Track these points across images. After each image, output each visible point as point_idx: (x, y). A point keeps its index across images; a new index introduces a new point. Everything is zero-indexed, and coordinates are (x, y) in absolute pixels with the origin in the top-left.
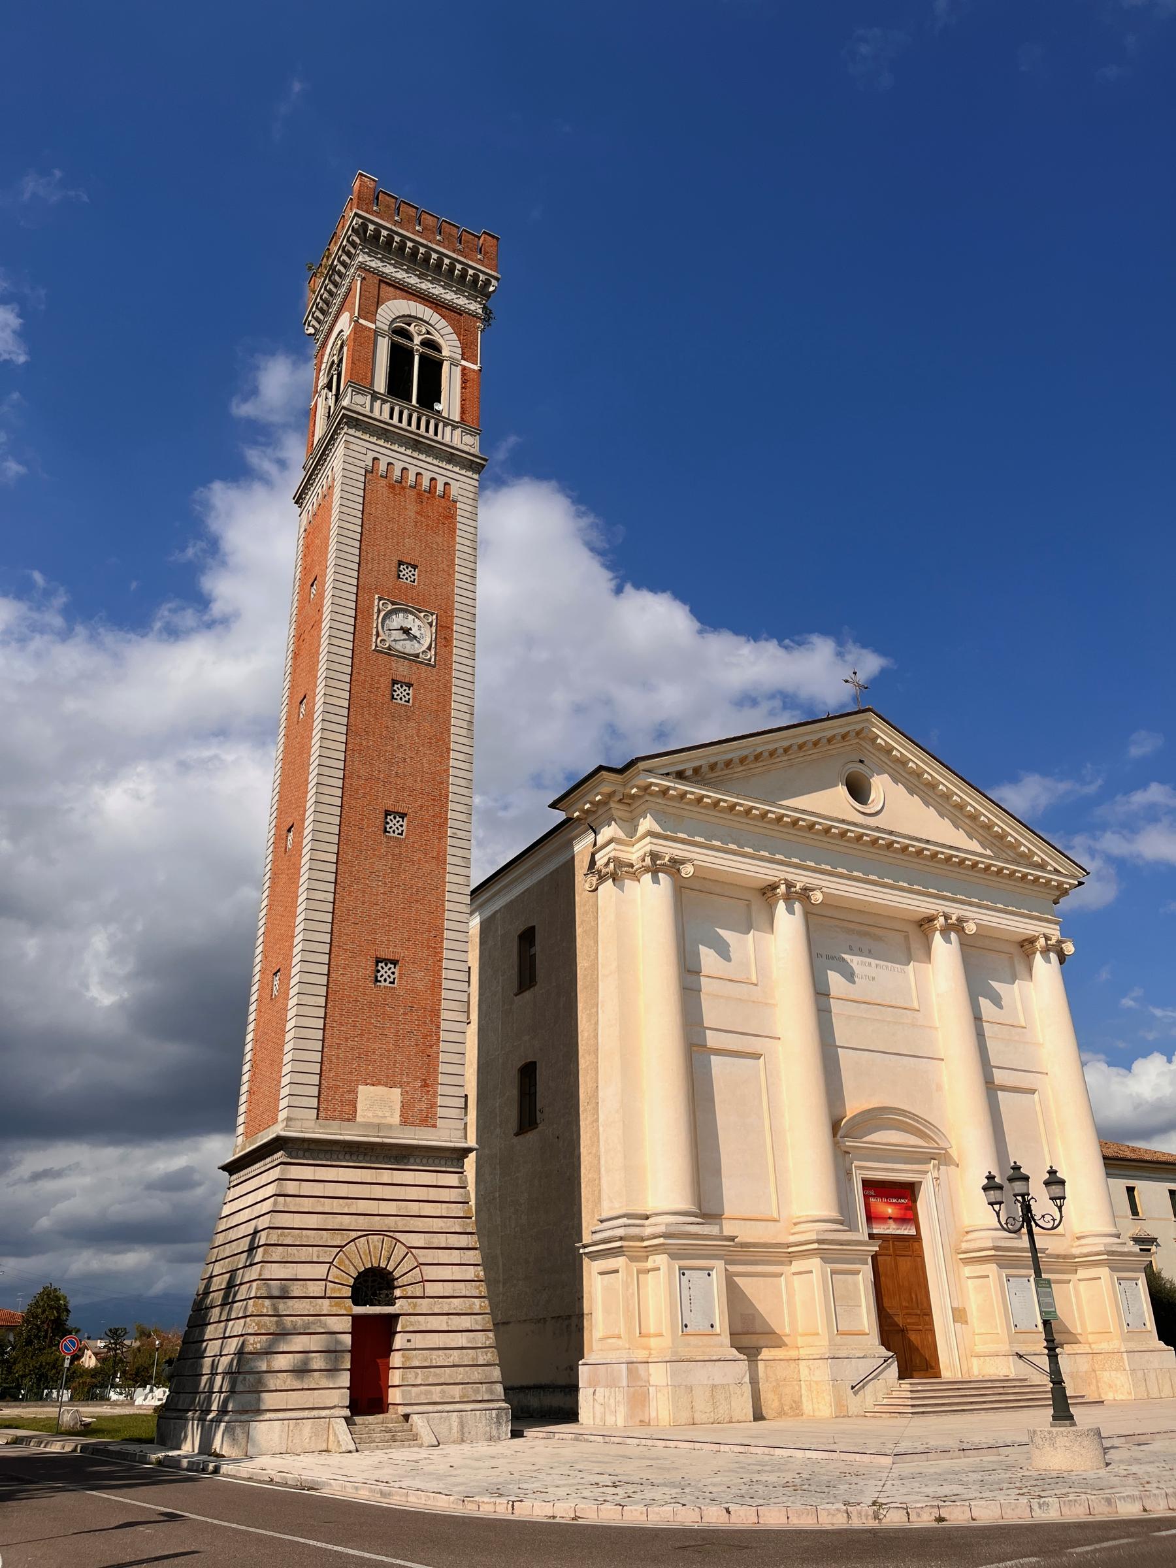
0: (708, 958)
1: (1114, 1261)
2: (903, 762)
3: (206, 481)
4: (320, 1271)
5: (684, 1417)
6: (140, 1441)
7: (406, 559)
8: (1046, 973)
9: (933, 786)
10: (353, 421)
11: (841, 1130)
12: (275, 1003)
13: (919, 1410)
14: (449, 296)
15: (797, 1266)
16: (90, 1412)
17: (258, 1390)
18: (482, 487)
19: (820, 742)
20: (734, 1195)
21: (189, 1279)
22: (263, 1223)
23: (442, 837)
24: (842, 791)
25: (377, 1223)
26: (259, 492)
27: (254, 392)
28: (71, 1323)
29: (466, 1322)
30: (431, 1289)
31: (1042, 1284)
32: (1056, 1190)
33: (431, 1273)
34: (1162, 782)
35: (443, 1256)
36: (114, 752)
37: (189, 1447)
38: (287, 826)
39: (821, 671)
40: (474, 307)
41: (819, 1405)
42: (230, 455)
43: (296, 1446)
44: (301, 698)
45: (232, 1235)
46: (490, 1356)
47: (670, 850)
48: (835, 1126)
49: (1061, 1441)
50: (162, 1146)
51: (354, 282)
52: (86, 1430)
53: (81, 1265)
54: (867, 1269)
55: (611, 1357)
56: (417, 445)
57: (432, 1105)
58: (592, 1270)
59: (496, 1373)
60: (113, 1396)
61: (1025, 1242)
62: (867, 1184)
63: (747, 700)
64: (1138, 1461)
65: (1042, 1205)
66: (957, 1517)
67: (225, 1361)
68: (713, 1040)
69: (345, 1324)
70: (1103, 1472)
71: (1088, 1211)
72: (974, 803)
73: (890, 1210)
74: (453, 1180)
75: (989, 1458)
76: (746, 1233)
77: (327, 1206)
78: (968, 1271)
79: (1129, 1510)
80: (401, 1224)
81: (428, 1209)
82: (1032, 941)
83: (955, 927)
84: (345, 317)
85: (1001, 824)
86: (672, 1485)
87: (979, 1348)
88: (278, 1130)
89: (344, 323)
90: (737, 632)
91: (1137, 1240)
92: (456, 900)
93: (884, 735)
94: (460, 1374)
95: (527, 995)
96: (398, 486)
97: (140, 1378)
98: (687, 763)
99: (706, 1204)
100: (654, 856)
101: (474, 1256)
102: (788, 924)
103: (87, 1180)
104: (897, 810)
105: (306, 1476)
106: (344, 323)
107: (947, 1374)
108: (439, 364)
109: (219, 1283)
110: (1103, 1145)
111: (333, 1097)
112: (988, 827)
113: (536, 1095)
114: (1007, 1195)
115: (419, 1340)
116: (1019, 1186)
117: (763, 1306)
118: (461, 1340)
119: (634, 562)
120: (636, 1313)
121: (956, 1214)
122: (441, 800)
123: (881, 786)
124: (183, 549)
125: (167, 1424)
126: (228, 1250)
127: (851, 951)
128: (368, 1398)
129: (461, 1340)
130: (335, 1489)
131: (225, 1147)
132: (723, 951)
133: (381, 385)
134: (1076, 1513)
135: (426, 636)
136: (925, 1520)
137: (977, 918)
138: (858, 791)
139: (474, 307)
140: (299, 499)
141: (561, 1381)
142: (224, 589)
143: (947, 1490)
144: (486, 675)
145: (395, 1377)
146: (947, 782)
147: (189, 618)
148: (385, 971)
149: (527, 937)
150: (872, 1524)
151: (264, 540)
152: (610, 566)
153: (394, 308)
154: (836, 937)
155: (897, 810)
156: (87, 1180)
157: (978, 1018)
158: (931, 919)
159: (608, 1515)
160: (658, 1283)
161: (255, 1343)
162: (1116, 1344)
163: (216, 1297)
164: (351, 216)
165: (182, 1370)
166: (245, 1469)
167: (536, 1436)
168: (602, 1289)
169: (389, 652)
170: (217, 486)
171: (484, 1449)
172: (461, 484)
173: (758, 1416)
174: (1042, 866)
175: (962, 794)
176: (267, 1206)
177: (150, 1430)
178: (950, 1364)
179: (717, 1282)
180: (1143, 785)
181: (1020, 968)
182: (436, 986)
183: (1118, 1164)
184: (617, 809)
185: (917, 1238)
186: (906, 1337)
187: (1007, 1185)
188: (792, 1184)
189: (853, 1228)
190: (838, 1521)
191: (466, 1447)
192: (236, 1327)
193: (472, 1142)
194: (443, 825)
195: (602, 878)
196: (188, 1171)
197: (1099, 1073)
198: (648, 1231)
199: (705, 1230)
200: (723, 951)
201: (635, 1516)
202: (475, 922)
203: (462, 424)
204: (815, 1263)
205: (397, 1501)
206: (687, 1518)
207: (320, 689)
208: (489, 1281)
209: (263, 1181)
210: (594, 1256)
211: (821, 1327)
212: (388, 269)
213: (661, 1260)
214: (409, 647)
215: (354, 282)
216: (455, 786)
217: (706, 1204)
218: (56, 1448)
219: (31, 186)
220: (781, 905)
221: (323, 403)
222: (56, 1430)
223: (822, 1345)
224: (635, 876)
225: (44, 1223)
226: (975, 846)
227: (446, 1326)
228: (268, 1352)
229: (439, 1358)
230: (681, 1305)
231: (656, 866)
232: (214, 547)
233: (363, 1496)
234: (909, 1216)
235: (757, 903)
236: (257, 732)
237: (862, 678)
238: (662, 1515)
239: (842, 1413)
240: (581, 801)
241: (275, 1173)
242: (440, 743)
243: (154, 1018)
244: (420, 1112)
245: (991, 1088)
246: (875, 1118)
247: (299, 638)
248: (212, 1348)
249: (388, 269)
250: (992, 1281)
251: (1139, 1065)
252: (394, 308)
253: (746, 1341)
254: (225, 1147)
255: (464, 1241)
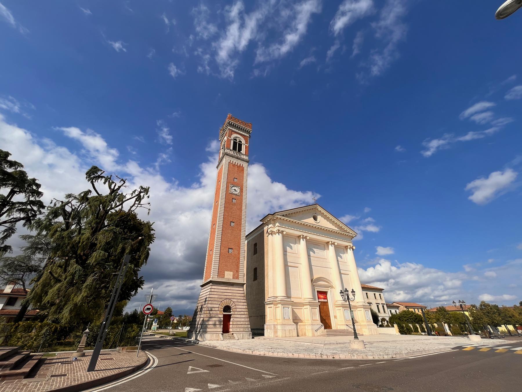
0: (288, 249)
1: (364, 307)
2: (323, 214)
3: (201, 163)
4: (217, 306)
5: (284, 335)
6: (184, 337)
7: (235, 177)
8: (350, 252)
9: (329, 218)
10: (227, 154)
11: (313, 281)
12: (211, 256)
13: (328, 335)
14: (243, 133)
15: (305, 307)
16: (175, 331)
17: (206, 328)
18: (248, 165)
19: (309, 210)
20: (293, 294)
21: (194, 306)
22: (207, 296)
23: (241, 226)
24: (312, 218)
25: (228, 297)
26: (211, 165)
27: (210, 147)
28: (172, 314)
29: (244, 316)
30: (238, 310)
31: (351, 311)
32: (353, 293)
33: (237, 307)
34: (371, 217)
35: (240, 304)
36: (183, 209)
37: (193, 339)
38: (214, 224)
39: (309, 197)
40: (247, 135)
41: (309, 334)
42: (205, 158)
43: (212, 339)
44: (216, 201)
45: (202, 298)
46: (248, 323)
47: (281, 229)
48: (312, 280)
49: (356, 343)
50: (189, 281)
51: (227, 131)
52: (174, 335)
53: (173, 303)
54: (318, 308)
55: (271, 324)
56: (237, 158)
57: (238, 275)
58: (267, 307)
59: (249, 326)
60: (179, 328)
61: (348, 303)
62: (318, 292)
63: (296, 202)
64: (371, 347)
65: (351, 296)
66: (337, 357)
67: (200, 322)
68: (289, 264)
69: (222, 316)
70: (365, 349)
71: (359, 298)
72: (336, 221)
73: (322, 297)
74: (242, 289)
75: (342, 345)
76: (296, 301)
77: (219, 293)
78: (337, 308)
79: (370, 358)
80: (232, 297)
81: (237, 295)
82: (347, 246)
83: (334, 244)
84: (226, 137)
85: (341, 225)
86: (282, 349)
87: (339, 324)
88: (210, 279)
89: (226, 138)
90: (294, 190)
91: (368, 303)
92: (243, 238)
93: (320, 209)
94: (243, 326)
95: (255, 255)
96: (234, 165)
97: (184, 325)
98: (284, 213)
99: (288, 295)
100: (279, 230)
101: (245, 304)
102: (303, 243)
103: (176, 287)
104: (322, 222)
105: (214, 345)
106: (226, 138)
107: (333, 328)
108: (241, 145)
109: (200, 307)
110: (361, 285)
111: (221, 273)
112: (339, 225)
113: (257, 274)
114: (344, 294)
115: (235, 319)
116: (347, 293)
117: (299, 315)
118: (243, 320)
119: (275, 177)
120: (275, 315)
121: (334, 298)
122: (241, 220)
123: (319, 218)
124: (198, 174)
125: (190, 332)
126: (201, 301)
127: (314, 248)
128: (226, 330)
129: (243, 320)
130: (220, 348)
131: (200, 282)
132: (291, 248)
133: (232, 148)
134: (360, 358)
135: (238, 191)
136: (331, 358)
137: (337, 242)
138: (315, 219)
139: (247, 135)
140: (217, 168)
141: (261, 328)
142: (204, 181)
143: (334, 352)
144: (249, 197)
145: (231, 326)
146: (331, 217)
147: (197, 186)
148: (230, 250)
149: (255, 245)
150: (321, 358)
151: (211, 172)
152: (271, 178)
153: (234, 136)
154: (311, 245)
155: (322, 222)
156: (176, 287)
157: (338, 261)
158: (329, 242)
159: (270, 354)
160: (279, 310)
161: (206, 319)
162: (365, 323)
163: (199, 310)
164: (227, 121)
165: (192, 323)
166: (203, 343)
167: (256, 338)
168: (269, 311)
169: (232, 193)
170: (203, 164)
171: (247, 340)
172: (245, 165)
173: (298, 336)
174: (349, 233)
175: (334, 219)
176: (208, 293)
177: (186, 335)
178: (334, 327)
179: (290, 309)
180: (367, 218)
181: (345, 251)
182: (239, 253)
183: (364, 288)
184: (272, 222)
185: (327, 302)
186: (325, 321)
187: (344, 292)
188: (304, 292)
189: (315, 300)
190: (314, 357)
191: (243, 340)
192: (202, 316)
193: (245, 282)
194: (241, 224)
195: (269, 234)
196: (194, 286)
197: (361, 271)
198: (277, 300)
199: (288, 300)
200: (291, 248)
201: (275, 355)
202: (246, 242)
203: (245, 155)
204: (308, 307)
205: (231, 350)
206: (285, 355)
207: (220, 200)
208: (248, 309)
209: (208, 287)
210: (267, 304)
211: (310, 319)
212: (233, 129)
213: (280, 305)
214: (236, 193)
215: (227, 131)
216: (243, 217)
217: (288, 295)
218: (169, 338)
219: (175, 114)
220: (302, 239)
221: (222, 151)
222: (169, 335)
223: (310, 322)
224: (275, 234)
225: (168, 295)
226: (336, 229)
227: (240, 317)
228: (208, 321)
229: (239, 323)
230: (283, 314)
231: (279, 232)
232: (203, 174)
233: (225, 349)
234: (326, 298)
235: (297, 239)
236: (210, 208)
237: (316, 199)
238: (280, 355)
239: (314, 336)
240: (266, 220)
241: (210, 287)
242: (240, 209)
243: (188, 258)
244: (236, 277)
245: (340, 273)
246: (319, 279)
247: (216, 191)
248: (198, 320)
249: (233, 129)
250: (341, 310)
251: (368, 269)
252: (234, 136)
253: (296, 321)
254: (200, 282)
255: (244, 301)
